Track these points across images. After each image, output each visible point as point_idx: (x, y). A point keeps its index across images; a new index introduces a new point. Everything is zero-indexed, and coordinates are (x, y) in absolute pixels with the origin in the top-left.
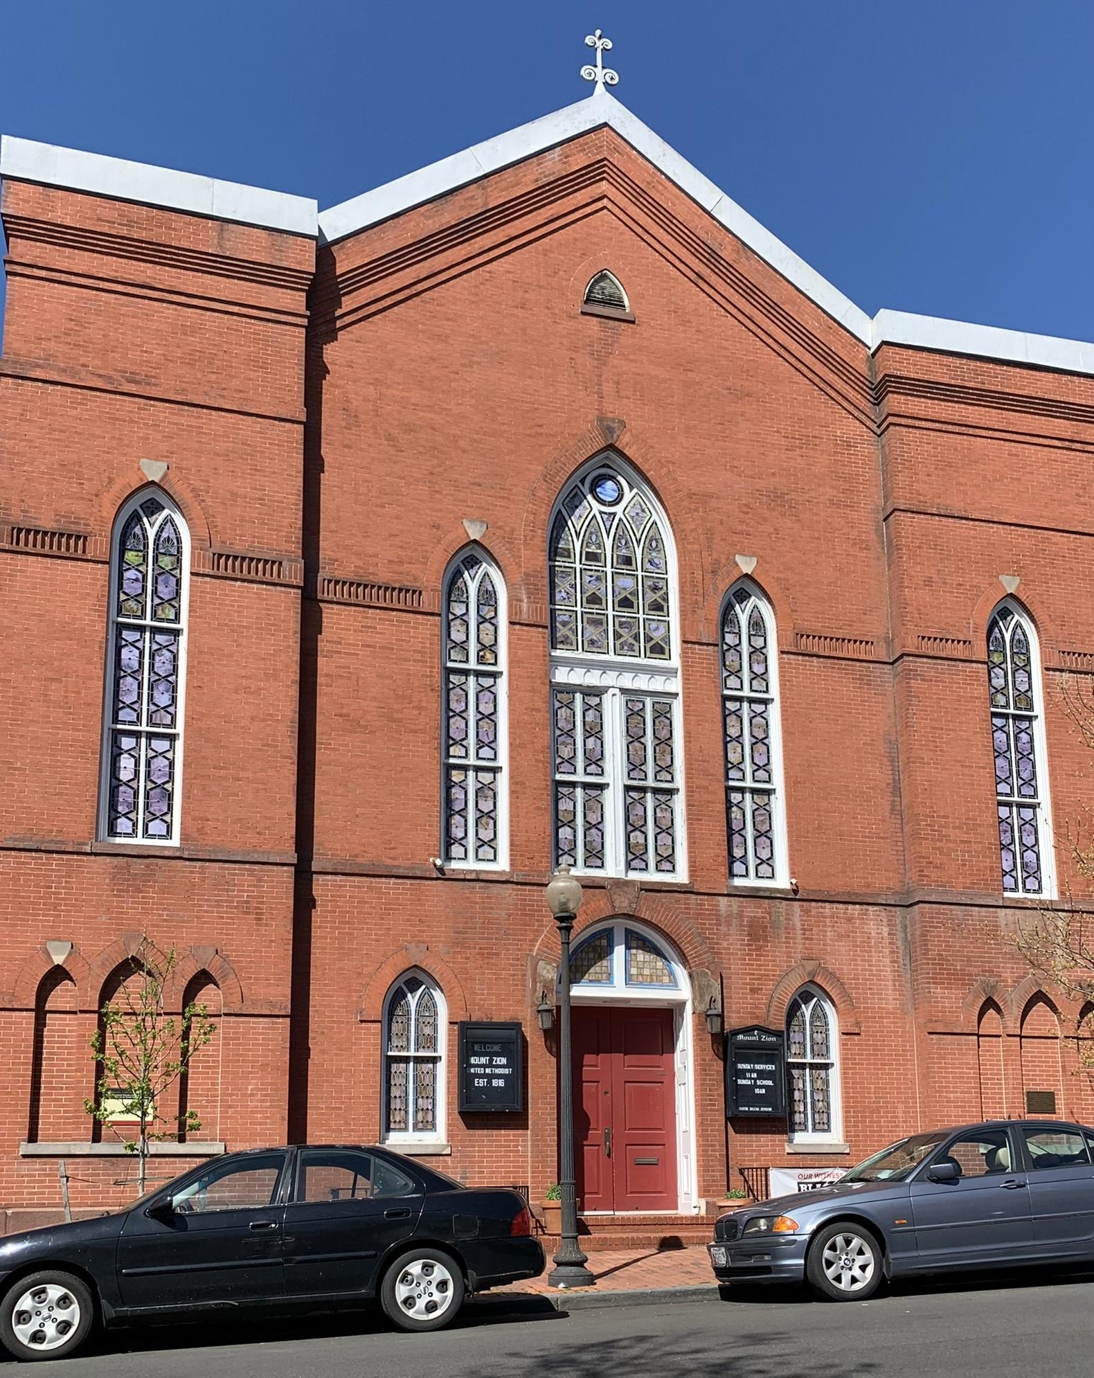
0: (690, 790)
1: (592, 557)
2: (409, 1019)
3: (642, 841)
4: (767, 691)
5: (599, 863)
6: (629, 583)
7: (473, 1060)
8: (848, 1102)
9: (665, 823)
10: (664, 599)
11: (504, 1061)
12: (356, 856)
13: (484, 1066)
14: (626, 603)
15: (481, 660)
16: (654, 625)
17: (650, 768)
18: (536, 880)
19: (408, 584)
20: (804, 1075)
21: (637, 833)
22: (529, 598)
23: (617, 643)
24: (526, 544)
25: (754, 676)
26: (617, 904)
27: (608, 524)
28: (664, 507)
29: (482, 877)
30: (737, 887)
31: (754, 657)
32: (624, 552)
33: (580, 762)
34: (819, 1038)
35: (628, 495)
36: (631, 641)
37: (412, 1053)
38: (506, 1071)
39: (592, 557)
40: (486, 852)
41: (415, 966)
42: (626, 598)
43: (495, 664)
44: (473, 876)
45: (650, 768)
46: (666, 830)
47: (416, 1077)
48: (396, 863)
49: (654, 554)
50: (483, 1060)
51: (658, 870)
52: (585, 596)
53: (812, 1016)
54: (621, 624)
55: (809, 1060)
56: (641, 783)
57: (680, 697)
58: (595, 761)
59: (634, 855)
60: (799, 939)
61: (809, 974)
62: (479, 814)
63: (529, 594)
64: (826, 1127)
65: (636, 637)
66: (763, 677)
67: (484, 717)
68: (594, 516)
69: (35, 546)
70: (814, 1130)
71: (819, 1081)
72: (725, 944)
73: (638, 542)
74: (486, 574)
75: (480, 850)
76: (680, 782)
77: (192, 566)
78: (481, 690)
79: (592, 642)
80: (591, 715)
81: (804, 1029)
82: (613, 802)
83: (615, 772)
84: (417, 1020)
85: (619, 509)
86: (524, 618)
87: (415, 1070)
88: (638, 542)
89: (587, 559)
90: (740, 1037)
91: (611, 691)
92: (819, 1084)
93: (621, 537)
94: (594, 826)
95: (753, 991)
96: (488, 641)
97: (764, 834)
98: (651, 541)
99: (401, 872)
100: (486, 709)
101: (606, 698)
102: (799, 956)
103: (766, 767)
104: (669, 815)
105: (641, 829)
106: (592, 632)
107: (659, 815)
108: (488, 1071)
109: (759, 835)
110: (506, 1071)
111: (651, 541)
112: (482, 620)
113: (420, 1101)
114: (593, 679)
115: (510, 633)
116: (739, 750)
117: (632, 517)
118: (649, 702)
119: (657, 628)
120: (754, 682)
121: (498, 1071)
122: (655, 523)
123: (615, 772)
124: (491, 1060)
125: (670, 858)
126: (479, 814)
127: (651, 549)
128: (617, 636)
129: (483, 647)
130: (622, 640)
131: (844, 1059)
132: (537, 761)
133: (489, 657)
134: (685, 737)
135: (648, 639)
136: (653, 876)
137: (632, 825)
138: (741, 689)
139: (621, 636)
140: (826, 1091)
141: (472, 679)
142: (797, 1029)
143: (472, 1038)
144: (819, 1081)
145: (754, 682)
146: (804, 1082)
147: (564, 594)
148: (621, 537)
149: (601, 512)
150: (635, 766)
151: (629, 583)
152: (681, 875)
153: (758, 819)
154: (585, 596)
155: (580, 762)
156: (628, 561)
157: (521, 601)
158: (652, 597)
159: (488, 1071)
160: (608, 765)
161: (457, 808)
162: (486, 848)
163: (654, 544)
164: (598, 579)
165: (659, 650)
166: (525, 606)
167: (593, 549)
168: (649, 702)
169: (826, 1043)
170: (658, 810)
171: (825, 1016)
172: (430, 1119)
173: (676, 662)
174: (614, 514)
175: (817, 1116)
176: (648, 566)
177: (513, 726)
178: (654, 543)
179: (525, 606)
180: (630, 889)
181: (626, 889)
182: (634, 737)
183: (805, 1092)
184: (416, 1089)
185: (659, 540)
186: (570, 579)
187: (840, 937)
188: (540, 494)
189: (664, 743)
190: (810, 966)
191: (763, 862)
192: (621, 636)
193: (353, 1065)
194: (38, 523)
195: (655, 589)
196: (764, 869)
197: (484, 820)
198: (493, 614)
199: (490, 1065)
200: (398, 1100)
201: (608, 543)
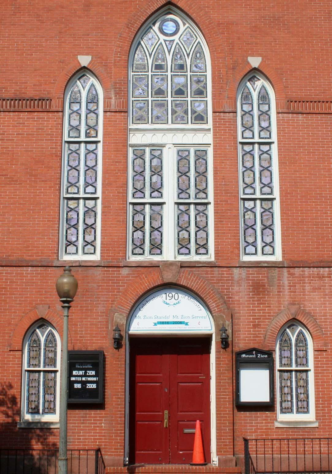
0: (216, 204)
1: (159, 67)
2: (40, 349)
3: (186, 236)
4: (270, 138)
5: (159, 252)
6: (182, 80)
7: (74, 373)
8: (319, 394)
9: (201, 225)
10: (204, 88)
11: (93, 373)
12: (9, 256)
13: (81, 376)
14: (180, 92)
15: (87, 135)
16: (197, 104)
17: (192, 191)
18: (115, 264)
19: (43, 96)
20: (291, 378)
21: (184, 232)
22: (116, 96)
23: (174, 117)
24: (115, 65)
25: (262, 129)
26: (165, 277)
27: (169, 47)
28: (202, 33)
29: (82, 264)
30: (244, 262)
31: (262, 117)
32: (180, 62)
33: (147, 192)
34: (301, 354)
35: (182, 28)
36: (183, 114)
37: (42, 368)
38: (95, 379)
39: (159, 67)
40: (89, 248)
41: (42, 318)
42: (180, 89)
43: (96, 136)
44: (77, 264)
45: (192, 191)
46: (202, 228)
47: (44, 382)
48: (31, 258)
49: (198, 61)
50: (81, 373)
51: (197, 253)
52: (154, 91)
53: (297, 340)
54: (176, 105)
55: (294, 367)
56: (206, 201)
57: (212, 146)
58: (157, 189)
59: (183, 245)
60: (287, 292)
61: (292, 314)
62: (85, 226)
63: (116, 94)
64: (306, 410)
65: (186, 112)
66: (268, 129)
67: (247, 169)
68: (161, 44)
69: (34, 107)
70: (298, 412)
71: (302, 381)
72: (237, 298)
73: (188, 55)
74: (93, 85)
75: (86, 248)
76: (211, 198)
77: (104, 107)
78: (89, 152)
79: (158, 118)
80: (155, 162)
81: (291, 348)
82: (169, 214)
83: (170, 194)
84: (45, 349)
85: (176, 38)
86: (113, 108)
87: (44, 377)
88: (188, 55)
89: (156, 69)
90: (244, 356)
91: (167, 146)
92: (301, 383)
93: (178, 53)
94: (157, 229)
95: (255, 326)
96: (92, 123)
97: (268, 227)
98: (196, 54)
99: (35, 263)
100: (91, 163)
101: (165, 150)
102: (287, 303)
103: (269, 185)
104: (204, 219)
105: (186, 229)
106: (157, 112)
107: (198, 219)
108: (84, 379)
109: (265, 227)
110: (95, 379)
111: (196, 54)
112: (89, 111)
113: (47, 396)
114: (157, 139)
115: (105, 117)
116: (252, 175)
117: (184, 41)
118: (148, 150)
119: (199, 106)
120: (262, 133)
121: (90, 379)
122: (199, 43)
123: (170, 194)
124: (86, 373)
125: (205, 246)
126: (85, 226)
127: (196, 58)
128: (174, 112)
129: (89, 127)
130: (177, 114)
131: (316, 367)
132: (118, 193)
133: (93, 133)
134: (214, 171)
135: (194, 112)
136: (194, 258)
137: (182, 227)
138: (253, 138)
139: (176, 112)
140: (306, 387)
141: (83, 145)
142: (286, 348)
143: (75, 359)
144: (302, 381)
145: (262, 133)
146: (291, 382)
147: (141, 91)
148: (178, 53)
149: (165, 41)
150: (182, 190)
151: (182, 80)
152: (211, 257)
153: (264, 218)
154: (154, 91)
155: (147, 192)
156: (181, 67)
157: (111, 98)
158: (195, 86)
159: (84, 379)
160: (165, 191)
161: (72, 224)
162: (89, 246)
163: (198, 55)
164: (162, 79)
165: (200, 118)
166: (113, 101)
167: (159, 62)
168: (148, 150)
169: (306, 357)
170: (198, 217)
171: (305, 340)
172: (52, 406)
173: (210, 125)
174: (173, 41)
175: (299, 403)
176: (194, 69)
177: (104, 172)
178: (198, 54)
179: (113, 101)
180: (174, 267)
181: (171, 267)
182: (182, 173)
183: (291, 389)
184: (44, 389)
185: (202, 53)
186: (145, 82)
187: (314, 289)
188: (125, 35)
189: (202, 174)
190: (294, 309)
191: (267, 244)
192: (176, 112)
193: (5, 376)
194: (44, 96)
195: (199, 81)
196: (268, 249)
197: (88, 230)
198: (96, 108)
199: (85, 376)
200: (34, 396)
201: (169, 58)
